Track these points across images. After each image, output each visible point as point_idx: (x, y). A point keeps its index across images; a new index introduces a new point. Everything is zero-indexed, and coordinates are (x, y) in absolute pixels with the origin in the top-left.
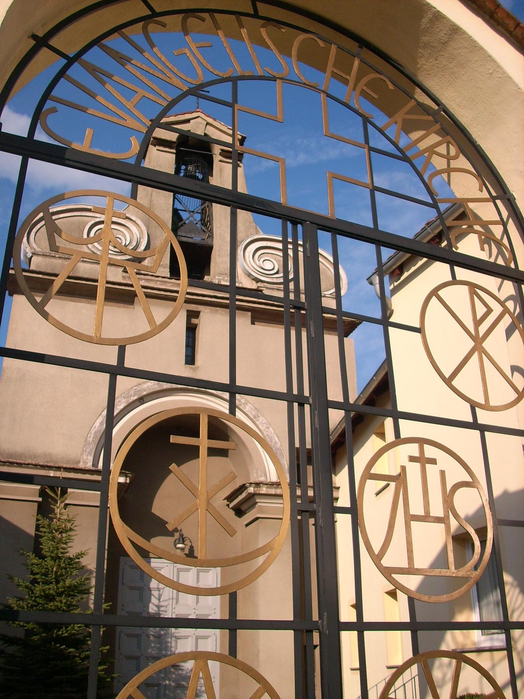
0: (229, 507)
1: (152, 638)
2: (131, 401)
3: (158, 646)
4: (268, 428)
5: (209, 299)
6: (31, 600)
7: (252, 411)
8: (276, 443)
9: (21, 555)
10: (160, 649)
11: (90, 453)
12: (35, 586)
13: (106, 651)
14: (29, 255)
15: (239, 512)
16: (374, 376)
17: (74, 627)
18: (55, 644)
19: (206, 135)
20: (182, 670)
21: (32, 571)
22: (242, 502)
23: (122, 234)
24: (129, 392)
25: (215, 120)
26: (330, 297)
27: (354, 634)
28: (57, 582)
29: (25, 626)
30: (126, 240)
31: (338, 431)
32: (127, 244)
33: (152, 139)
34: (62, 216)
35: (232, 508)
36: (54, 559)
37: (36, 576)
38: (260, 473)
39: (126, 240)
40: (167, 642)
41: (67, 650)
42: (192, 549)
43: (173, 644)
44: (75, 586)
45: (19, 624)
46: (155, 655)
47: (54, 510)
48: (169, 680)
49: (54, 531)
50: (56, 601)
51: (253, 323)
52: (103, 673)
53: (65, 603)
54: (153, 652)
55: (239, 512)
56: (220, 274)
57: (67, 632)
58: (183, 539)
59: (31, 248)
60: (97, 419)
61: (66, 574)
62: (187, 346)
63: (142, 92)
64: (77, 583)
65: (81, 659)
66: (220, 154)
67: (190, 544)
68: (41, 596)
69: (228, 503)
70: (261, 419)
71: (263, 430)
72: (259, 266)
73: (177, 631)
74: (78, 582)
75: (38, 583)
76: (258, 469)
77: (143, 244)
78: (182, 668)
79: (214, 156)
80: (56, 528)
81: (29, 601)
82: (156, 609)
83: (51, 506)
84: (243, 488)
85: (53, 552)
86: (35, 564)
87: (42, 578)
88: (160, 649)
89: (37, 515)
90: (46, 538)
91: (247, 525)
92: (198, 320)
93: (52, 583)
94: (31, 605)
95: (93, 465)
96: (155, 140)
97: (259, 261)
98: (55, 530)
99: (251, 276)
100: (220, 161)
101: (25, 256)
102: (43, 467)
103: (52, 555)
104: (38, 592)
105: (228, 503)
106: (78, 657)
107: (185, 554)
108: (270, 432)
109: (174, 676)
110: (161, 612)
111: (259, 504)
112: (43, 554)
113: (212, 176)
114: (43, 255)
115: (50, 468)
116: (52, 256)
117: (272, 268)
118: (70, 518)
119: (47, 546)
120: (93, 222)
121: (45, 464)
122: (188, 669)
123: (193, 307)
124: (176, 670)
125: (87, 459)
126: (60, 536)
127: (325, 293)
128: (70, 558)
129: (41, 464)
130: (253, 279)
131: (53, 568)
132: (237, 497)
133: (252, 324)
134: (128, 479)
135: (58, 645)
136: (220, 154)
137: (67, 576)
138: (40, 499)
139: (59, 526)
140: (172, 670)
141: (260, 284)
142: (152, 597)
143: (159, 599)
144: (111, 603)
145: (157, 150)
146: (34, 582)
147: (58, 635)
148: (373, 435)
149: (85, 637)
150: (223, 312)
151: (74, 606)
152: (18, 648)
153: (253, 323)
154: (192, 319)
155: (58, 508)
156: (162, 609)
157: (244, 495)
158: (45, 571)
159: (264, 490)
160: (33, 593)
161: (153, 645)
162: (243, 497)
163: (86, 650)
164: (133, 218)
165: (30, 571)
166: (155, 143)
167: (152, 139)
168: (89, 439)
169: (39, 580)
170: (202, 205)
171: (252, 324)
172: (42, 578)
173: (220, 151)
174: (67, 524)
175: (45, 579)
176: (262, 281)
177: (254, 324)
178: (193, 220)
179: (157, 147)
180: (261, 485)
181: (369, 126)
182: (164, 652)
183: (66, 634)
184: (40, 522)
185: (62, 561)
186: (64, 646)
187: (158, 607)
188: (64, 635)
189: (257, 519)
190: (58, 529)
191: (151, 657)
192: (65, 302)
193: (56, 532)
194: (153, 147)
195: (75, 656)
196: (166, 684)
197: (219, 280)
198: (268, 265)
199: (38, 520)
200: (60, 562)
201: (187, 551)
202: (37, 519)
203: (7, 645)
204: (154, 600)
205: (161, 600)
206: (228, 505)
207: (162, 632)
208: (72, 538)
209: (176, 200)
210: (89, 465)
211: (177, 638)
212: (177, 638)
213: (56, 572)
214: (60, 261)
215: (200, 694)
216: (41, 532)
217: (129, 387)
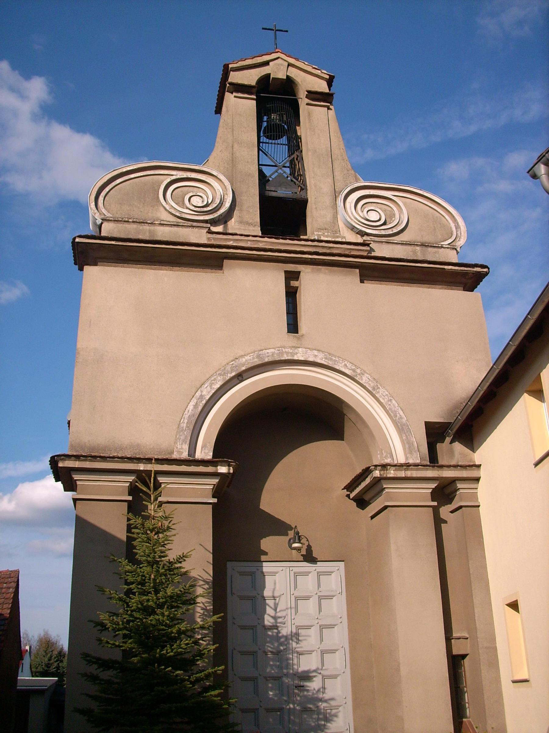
0: (349, 498)
1: (270, 655)
2: (228, 378)
3: (278, 663)
4: (391, 400)
5: (310, 256)
6: (127, 614)
7: (370, 383)
8: (401, 418)
9: (112, 561)
10: (280, 668)
11: (184, 441)
12: (130, 598)
13: (221, 672)
14: (99, 221)
15: (362, 502)
16: (528, 314)
17: (180, 645)
18: (159, 665)
19: (287, 76)
20: (308, 691)
21: (126, 580)
22: (365, 490)
23: (203, 191)
24: (225, 369)
25: (297, 59)
26: (448, 248)
28: (157, 592)
29: (122, 646)
30: (208, 198)
31: (479, 393)
32: (210, 202)
33: (228, 85)
34: (132, 176)
35: (354, 499)
36: (153, 563)
37: (131, 586)
38: (385, 454)
39: (208, 198)
40: (288, 659)
41: (174, 673)
42: (309, 548)
43: (295, 661)
44: (178, 596)
45: (114, 644)
46: (275, 675)
47: (147, 506)
48: (294, 704)
49: (149, 532)
50: (157, 615)
51: (362, 281)
52: (219, 698)
53: (168, 616)
54: (273, 671)
55: (362, 502)
56: (319, 229)
57: (172, 652)
58: (299, 537)
59: (100, 214)
60: (190, 401)
61: (166, 582)
62: (288, 313)
64: (181, 591)
65: (191, 683)
67: (307, 543)
68: (138, 610)
69: (349, 493)
70: (381, 390)
71: (384, 404)
72: (362, 218)
73: (298, 645)
74: (182, 589)
75: (134, 594)
76: (382, 450)
77: (228, 201)
78: (308, 688)
79: (300, 101)
80: (151, 527)
81: (125, 616)
82: (272, 620)
83: (144, 502)
84: (367, 472)
85: (149, 556)
86: (128, 572)
87: (138, 588)
88: (280, 668)
89: (128, 513)
90: (140, 540)
91: (372, 517)
92: (298, 282)
93: (150, 593)
94: (127, 620)
95: (189, 455)
96: (232, 86)
97: (362, 212)
98: (150, 530)
99: (355, 230)
100: (307, 104)
101: (95, 223)
102: (131, 459)
103: (149, 559)
104: (135, 604)
105: (349, 493)
106: (188, 680)
107: (302, 555)
108: (394, 405)
109: (298, 698)
110: (278, 625)
111: (387, 490)
112: (137, 559)
113: (299, 125)
114: (114, 221)
115: (139, 460)
116: (125, 221)
117: (378, 218)
118: (167, 514)
119: (141, 550)
120: (169, 180)
121: (134, 456)
122: (314, 689)
124: (301, 691)
125: (182, 448)
126: (156, 537)
127: (442, 243)
128: (170, 563)
129: (129, 456)
130: (357, 233)
131: (150, 575)
132: (360, 484)
133: (361, 282)
134: (231, 468)
135: (163, 667)
136: (307, 97)
137: (168, 584)
138: (130, 498)
139: (154, 524)
140: (296, 691)
141: (365, 238)
142: (267, 607)
143: (275, 610)
144: (223, 614)
145: (235, 97)
146: (129, 593)
147: (161, 655)
148: (525, 394)
149: (194, 656)
150: (327, 271)
151: (178, 619)
152: (115, 672)
153: (362, 281)
154: (291, 282)
155: (152, 504)
156: (279, 620)
157: (368, 480)
158: (142, 579)
159: (392, 473)
160: (128, 606)
161: (271, 663)
162: (367, 483)
163: (195, 672)
165: (123, 581)
166: (232, 90)
167: (228, 85)
168: (182, 425)
169: (135, 591)
170: (290, 156)
171: (361, 282)
172: (138, 588)
173: (307, 93)
174: (164, 522)
175: (141, 589)
176: (368, 234)
177: (364, 283)
178: (282, 172)
179: (235, 94)
180: (389, 467)
182: (285, 671)
183: (172, 654)
184: (131, 522)
185: (161, 567)
186: (170, 668)
187: (275, 618)
188: (168, 655)
189: (386, 507)
190: (154, 529)
191: (269, 677)
192: (143, 270)
193: (151, 532)
195: (183, 680)
196: (290, 708)
197: (318, 235)
198: (373, 216)
199: (129, 520)
200: (159, 568)
201: (304, 552)
202: (128, 518)
203: (102, 669)
204: (269, 611)
205: (278, 610)
206: (348, 496)
207: (282, 648)
208: (170, 539)
209: (260, 152)
210: (185, 455)
211: (300, 654)
212: (300, 654)
213: (154, 580)
214: (135, 226)
215: (330, 718)
216: (133, 533)
217: (224, 363)
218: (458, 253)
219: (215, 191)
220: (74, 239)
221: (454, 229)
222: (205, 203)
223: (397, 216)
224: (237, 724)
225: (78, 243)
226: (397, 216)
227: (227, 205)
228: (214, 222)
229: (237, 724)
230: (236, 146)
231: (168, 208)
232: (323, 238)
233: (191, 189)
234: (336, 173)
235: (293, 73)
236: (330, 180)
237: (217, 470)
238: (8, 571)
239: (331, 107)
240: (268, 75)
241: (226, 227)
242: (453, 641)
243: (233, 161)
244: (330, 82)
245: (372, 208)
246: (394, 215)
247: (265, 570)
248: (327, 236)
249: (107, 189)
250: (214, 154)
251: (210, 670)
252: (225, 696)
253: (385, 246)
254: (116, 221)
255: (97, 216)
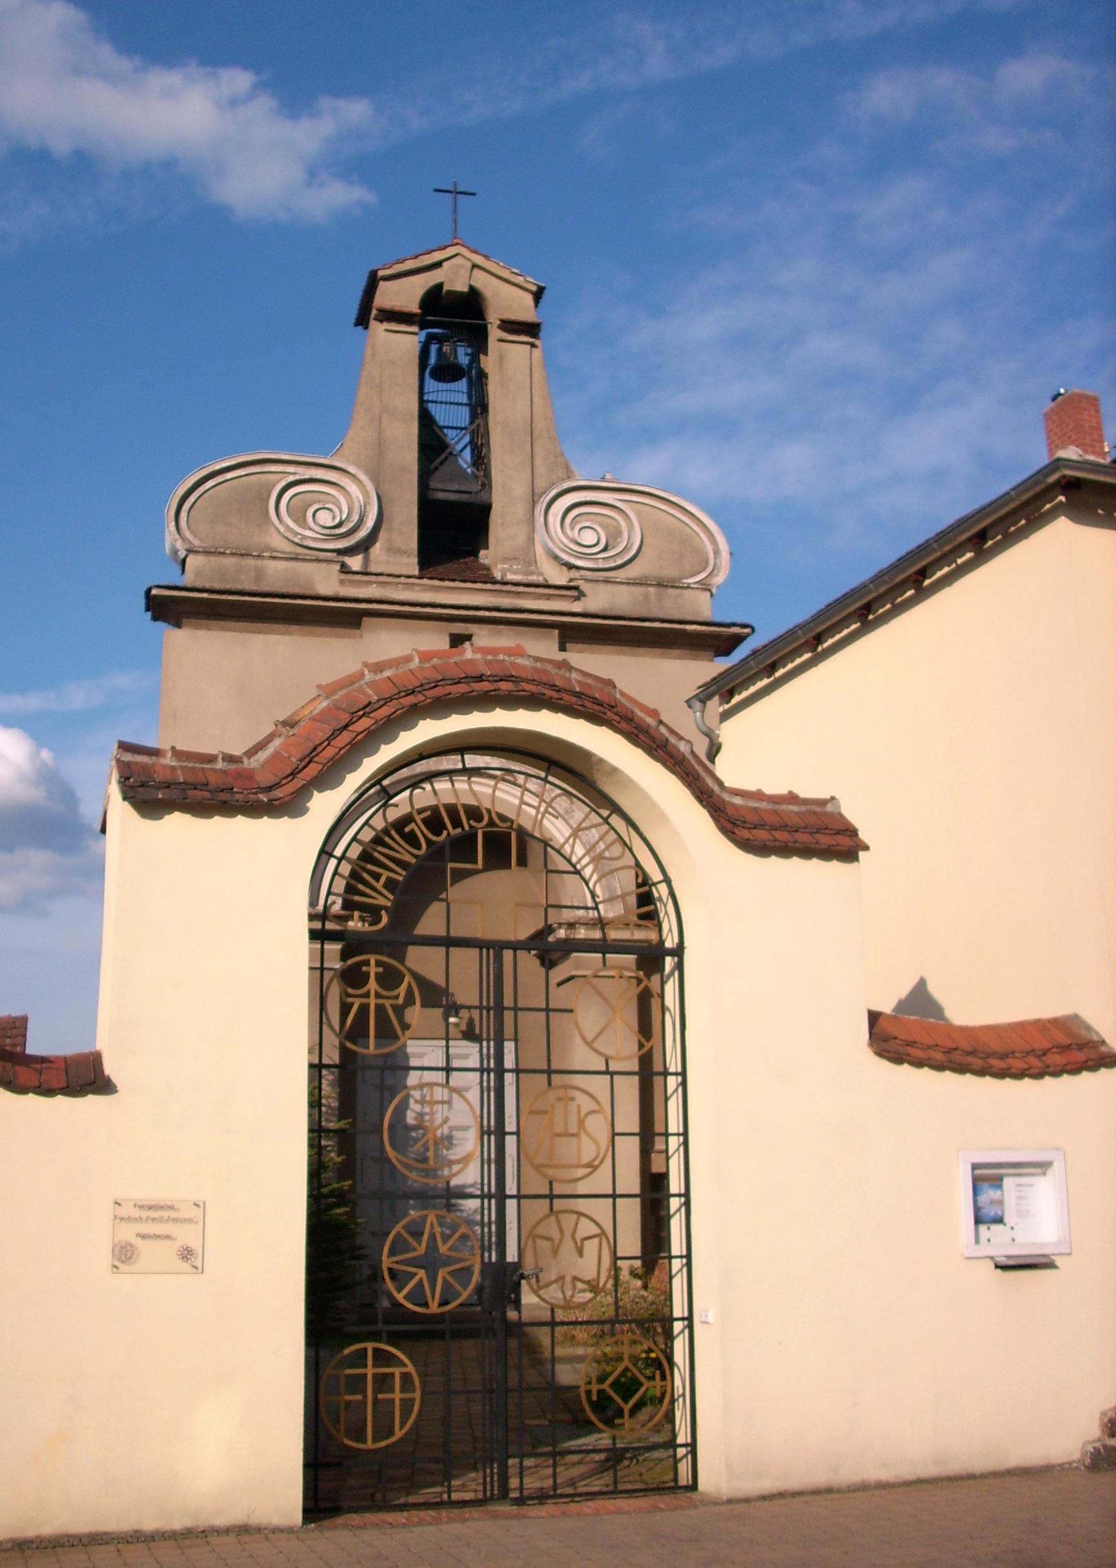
19: (472, 288)
20: (461, 1211)
25: (487, 257)
27: (515, 1201)
32: (344, 517)
34: (229, 475)
56: (505, 560)
63: (385, 874)
66: (499, 327)
97: (572, 529)
113: (486, 354)
120: (283, 484)
123: (460, 628)
136: (499, 327)
141: (574, 574)
164: (352, 469)
176: (578, 568)
179: (386, 325)
181: (549, 849)
189: (572, 978)
194: (378, 324)
198: (588, 538)
201: (464, 1027)
214: (234, 560)
218: (712, 595)
219: (350, 498)
220: (149, 590)
221: (711, 555)
222: (337, 521)
223: (625, 535)
224: (364, 1248)
225: (155, 596)
226: (625, 535)
227: (370, 523)
228: (350, 551)
229: (364, 1248)
230: (385, 420)
231: (282, 530)
232: (510, 577)
233: (316, 496)
234: (538, 461)
235: (481, 281)
236: (527, 476)
237: (346, 926)
238: (10, 1017)
239: (537, 342)
240: (440, 286)
241: (366, 561)
242: (653, 1155)
243: (380, 445)
244: (538, 295)
245: (588, 524)
246: (621, 533)
247: (409, 1050)
248: (515, 573)
249: (192, 499)
250: (352, 433)
251: (335, 1186)
252: (352, 1215)
253: (602, 588)
254: (207, 552)
255: (179, 545)
